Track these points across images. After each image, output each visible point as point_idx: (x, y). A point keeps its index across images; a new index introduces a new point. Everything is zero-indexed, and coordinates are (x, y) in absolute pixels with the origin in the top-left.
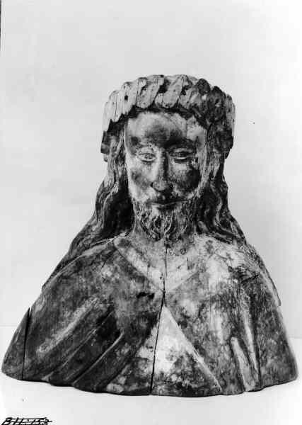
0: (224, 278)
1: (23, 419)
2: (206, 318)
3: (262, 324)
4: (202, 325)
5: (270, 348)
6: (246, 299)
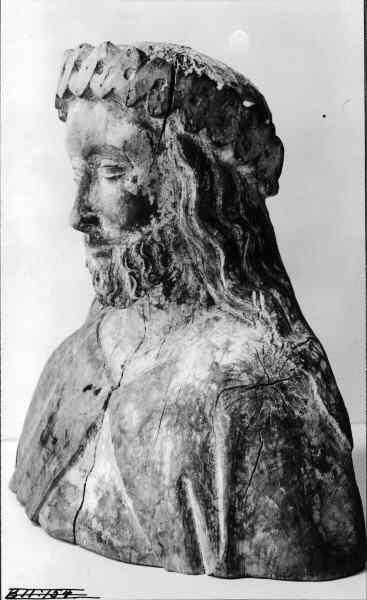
0: (197, 379)
1: (34, 590)
2: (149, 437)
3: (251, 468)
4: (141, 448)
5: (263, 513)
6: (224, 420)
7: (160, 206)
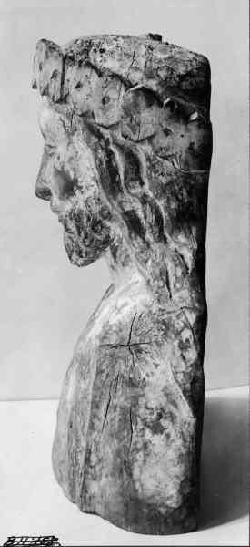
7: (79, 179)
